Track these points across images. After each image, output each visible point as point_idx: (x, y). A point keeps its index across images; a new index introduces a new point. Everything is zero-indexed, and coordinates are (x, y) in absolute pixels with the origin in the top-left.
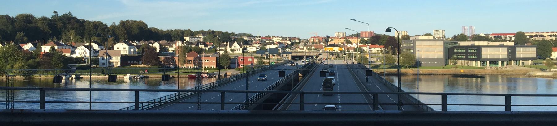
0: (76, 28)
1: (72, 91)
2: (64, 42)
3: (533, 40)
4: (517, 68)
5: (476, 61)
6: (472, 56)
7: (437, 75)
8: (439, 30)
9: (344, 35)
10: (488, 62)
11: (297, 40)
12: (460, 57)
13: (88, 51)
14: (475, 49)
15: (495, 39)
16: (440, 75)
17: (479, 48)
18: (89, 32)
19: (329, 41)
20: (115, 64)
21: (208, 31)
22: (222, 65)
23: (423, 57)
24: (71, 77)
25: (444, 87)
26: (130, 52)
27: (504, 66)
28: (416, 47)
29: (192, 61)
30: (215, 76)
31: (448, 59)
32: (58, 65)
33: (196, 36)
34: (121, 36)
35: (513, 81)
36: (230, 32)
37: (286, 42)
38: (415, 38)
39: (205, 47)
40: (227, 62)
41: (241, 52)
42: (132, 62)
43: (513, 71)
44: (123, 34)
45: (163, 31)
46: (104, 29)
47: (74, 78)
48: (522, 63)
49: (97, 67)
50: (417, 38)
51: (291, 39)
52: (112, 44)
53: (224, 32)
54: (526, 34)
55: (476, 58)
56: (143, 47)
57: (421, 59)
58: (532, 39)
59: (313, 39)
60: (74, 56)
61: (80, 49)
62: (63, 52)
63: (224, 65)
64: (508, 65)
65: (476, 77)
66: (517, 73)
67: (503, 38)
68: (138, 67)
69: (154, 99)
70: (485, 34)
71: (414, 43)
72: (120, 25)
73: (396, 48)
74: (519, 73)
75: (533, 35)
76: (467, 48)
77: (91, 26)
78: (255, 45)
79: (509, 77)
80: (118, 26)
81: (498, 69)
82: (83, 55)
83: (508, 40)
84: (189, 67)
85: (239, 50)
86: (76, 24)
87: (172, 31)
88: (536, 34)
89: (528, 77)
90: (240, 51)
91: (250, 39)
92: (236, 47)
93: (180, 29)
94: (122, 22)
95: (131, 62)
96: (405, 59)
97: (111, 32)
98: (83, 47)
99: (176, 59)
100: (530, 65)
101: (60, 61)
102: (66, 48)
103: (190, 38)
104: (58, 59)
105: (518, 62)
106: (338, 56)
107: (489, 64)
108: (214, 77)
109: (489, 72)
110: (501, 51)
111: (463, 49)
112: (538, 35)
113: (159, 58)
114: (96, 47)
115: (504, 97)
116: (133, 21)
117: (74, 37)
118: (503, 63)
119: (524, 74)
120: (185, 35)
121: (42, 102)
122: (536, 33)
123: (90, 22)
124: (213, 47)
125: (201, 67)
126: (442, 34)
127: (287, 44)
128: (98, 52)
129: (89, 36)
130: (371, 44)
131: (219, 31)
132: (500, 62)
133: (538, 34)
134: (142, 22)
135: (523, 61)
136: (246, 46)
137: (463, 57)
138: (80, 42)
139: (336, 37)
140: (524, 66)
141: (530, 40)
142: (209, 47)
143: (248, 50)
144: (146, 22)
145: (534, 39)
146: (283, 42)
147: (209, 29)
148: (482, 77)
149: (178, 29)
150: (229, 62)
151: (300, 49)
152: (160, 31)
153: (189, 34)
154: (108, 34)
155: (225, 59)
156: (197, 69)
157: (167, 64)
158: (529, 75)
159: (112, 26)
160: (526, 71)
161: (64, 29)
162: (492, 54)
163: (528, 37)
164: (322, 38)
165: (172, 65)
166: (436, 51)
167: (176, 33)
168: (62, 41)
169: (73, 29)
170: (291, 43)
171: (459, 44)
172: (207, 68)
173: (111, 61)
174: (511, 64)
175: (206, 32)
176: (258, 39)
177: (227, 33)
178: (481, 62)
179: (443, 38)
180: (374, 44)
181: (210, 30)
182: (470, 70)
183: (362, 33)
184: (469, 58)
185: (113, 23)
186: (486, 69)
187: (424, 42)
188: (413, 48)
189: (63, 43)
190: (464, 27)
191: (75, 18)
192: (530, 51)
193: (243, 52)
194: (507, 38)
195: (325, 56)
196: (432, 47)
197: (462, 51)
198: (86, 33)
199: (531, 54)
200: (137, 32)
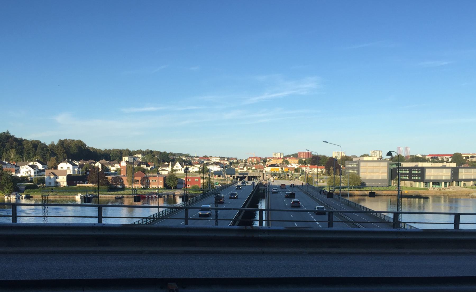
0: (14, 147)
1: (107, 208)
2: (7, 161)
3: (470, 161)
4: (459, 189)
5: (419, 182)
6: (416, 177)
7: (382, 195)
8: (376, 151)
9: (282, 155)
10: (431, 183)
11: (235, 160)
12: (403, 178)
13: (32, 171)
14: (419, 170)
15: (432, 160)
16: (385, 195)
17: (423, 170)
18: (28, 151)
19: (267, 162)
20: (61, 183)
21: (146, 151)
22: (169, 185)
23: (367, 178)
24: (21, 197)
25: (387, 206)
26: (74, 171)
27: (447, 187)
28: (361, 168)
29: (140, 181)
30: (164, 196)
31: (391, 180)
32: (7, 184)
33: (135, 156)
34: (60, 155)
35: (454, 202)
36: (168, 152)
37: (224, 162)
38: (359, 159)
39: (147, 167)
40: (175, 183)
41: (183, 172)
42: (78, 182)
43: (455, 192)
44: (62, 153)
45: (102, 151)
46: (43, 148)
47: (24, 197)
48: (464, 184)
49: (44, 186)
50: (361, 159)
51: (229, 159)
52: (55, 164)
53: (162, 151)
54: (463, 155)
55: (419, 179)
56: (86, 167)
57: (366, 179)
58: (469, 160)
59: (251, 159)
60: (19, 175)
61: (25, 168)
62: (11, 171)
63: (171, 185)
64: (450, 186)
65: (419, 197)
66: (460, 194)
67: (440, 159)
68: (87, 187)
69: (153, 214)
70: (422, 155)
71: (359, 165)
72: (59, 144)
73: (337, 169)
74: (462, 194)
75: (470, 156)
76: (410, 169)
77: (29, 145)
78: (196, 165)
79: (451, 197)
80: (56, 145)
81: (441, 190)
82: (27, 175)
83: (445, 161)
84: (137, 188)
85: (181, 170)
86: (14, 142)
87: (110, 150)
88: (472, 155)
89: (472, 198)
90: (182, 171)
91: (189, 159)
92: (178, 167)
93: (118, 149)
94: (60, 141)
95: (76, 182)
96: (351, 180)
97: (50, 151)
98: (27, 166)
99: (123, 179)
100: (471, 186)
101: (9, 180)
102: (10, 167)
103: (128, 158)
104: (7, 179)
105: (460, 183)
106: (279, 176)
107: (432, 185)
108: (163, 197)
109: (432, 192)
110: (444, 172)
111: (407, 170)
112: (474, 156)
113: (107, 178)
114: (40, 166)
115: (454, 215)
116: (71, 140)
117: (15, 156)
118: (446, 183)
119: (467, 195)
120: (123, 154)
121: (100, 217)
122: (472, 154)
123: (28, 141)
124: (155, 167)
125: (148, 187)
126: (379, 155)
127: (226, 164)
128: (43, 171)
129: (28, 155)
130: (311, 165)
131: (157, 151)
132: (443, 183)
133: (474, 155)
134: (81, 141)
135: (465, 182)
136: (187, 166)
137: (406, 178)
138: (22, 161)
139: (274, 157)
140: (466, 187)
141: (466, 161)
142: (151, 167)
143: (190, 170)
144: (84, 142)
145: (470, 160)
146: (222, 162)
147: (147, 149)
148: (426, 198)
149: (117, 148)
150: (176, 182)
151: (241, 169)
152: (97, 151)
153: (127, 153)
154: (47, 153)
155: (172, 180)
156: (144, 189)
157: (115, 184)
158: (472, 196)
159: (51, 145)
160: (469, 192)
161: (2, 148)
162: (436, 175)
163: (464, 158)
164: (260, 159)
165: (120, 184)
166: (380, 172)
167: (114, 152)
168: (5, 160)
169: (12, 147)
170: (229, 163)
171: (403, 165)
172: (154, 188)
173: (57, 180)
174: (453, 185)
175: (144, 151)
176: (196, 159)
177: (165, 153)
178: (425, 183)
179: (380, 159)
180: (314, 165)
181: (148, 149)
182: (414, 191)
183: (300, 153)
184: (413, 179)
185: (52, 142)
186: (429, 190)
187: (369, 163)
188: (358, 169)
189: (7, 162)
190: (399, 148)
191: (13, 136)
192: (472, 173)
193: (185, 172)
194: (444, 159)
195: (268, 177)
196: (377, 168)
197: (406, 172)
198: (25, 152)
199: (473, 175)
200: (76, 151)
